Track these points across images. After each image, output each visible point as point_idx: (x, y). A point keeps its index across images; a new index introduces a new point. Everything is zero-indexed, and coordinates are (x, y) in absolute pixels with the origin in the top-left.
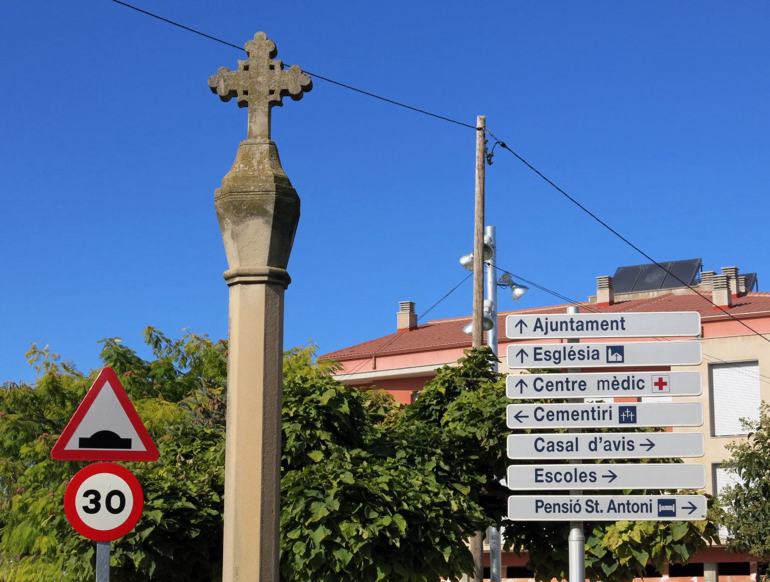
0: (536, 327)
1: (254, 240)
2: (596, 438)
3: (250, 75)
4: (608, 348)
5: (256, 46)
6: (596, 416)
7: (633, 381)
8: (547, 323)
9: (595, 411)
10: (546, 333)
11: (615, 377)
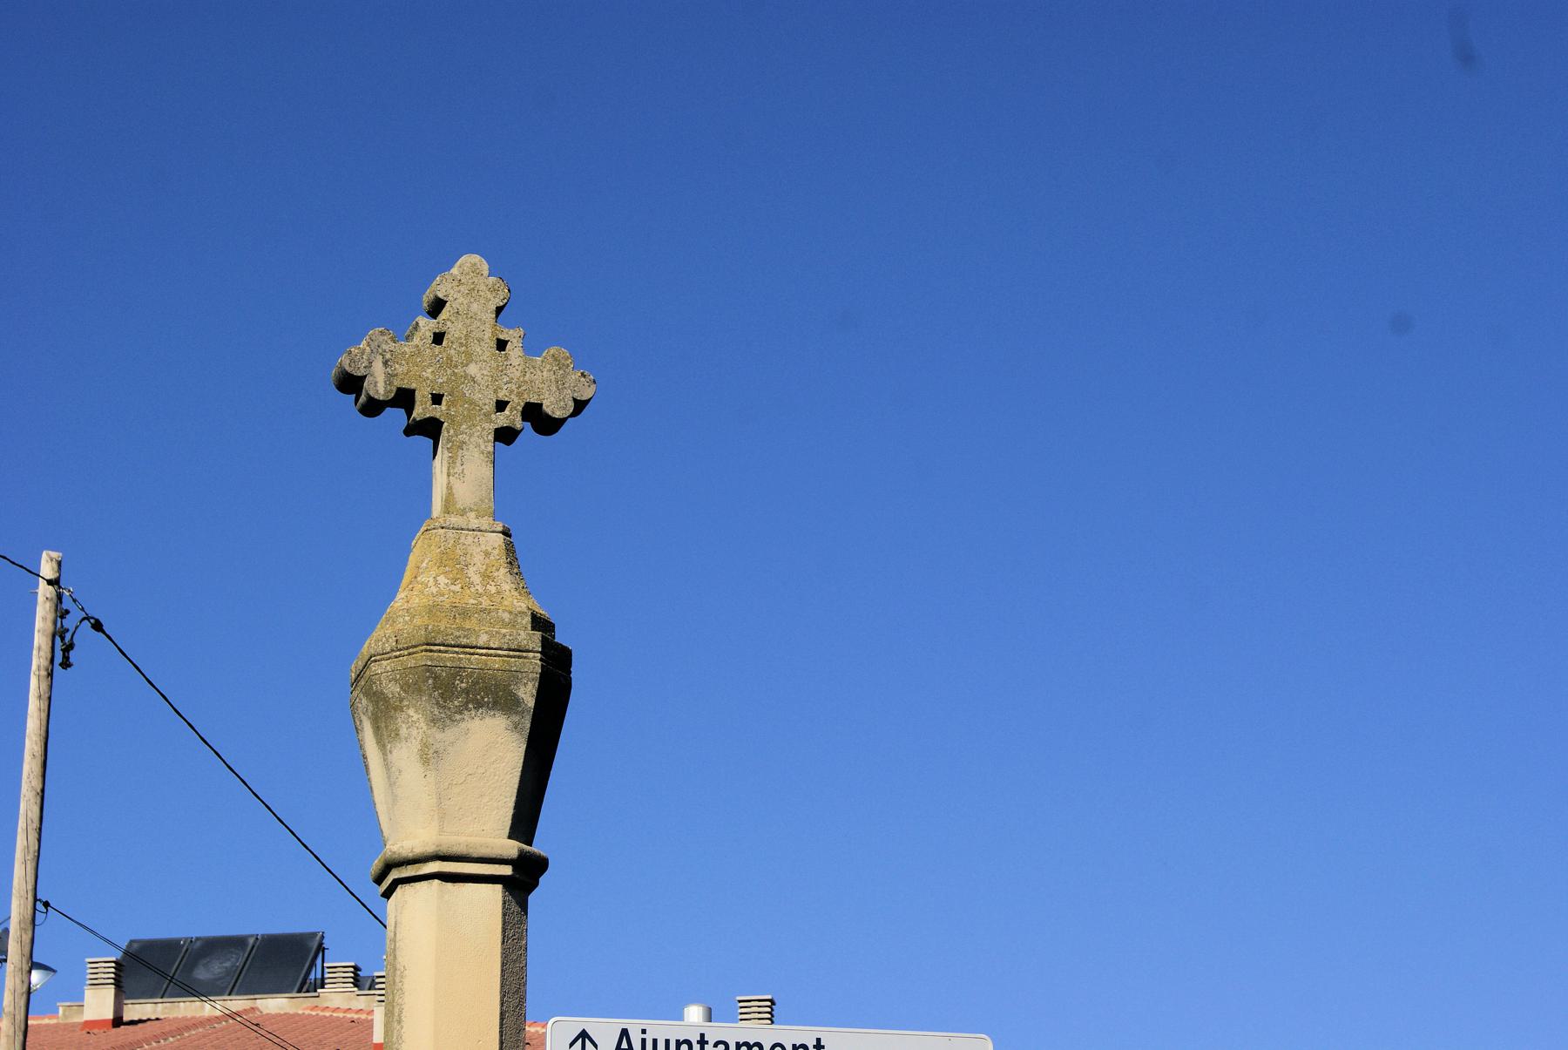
1: (481, 770)
3: (450, 358)
5: (462, 288)
8: (644, 1041)
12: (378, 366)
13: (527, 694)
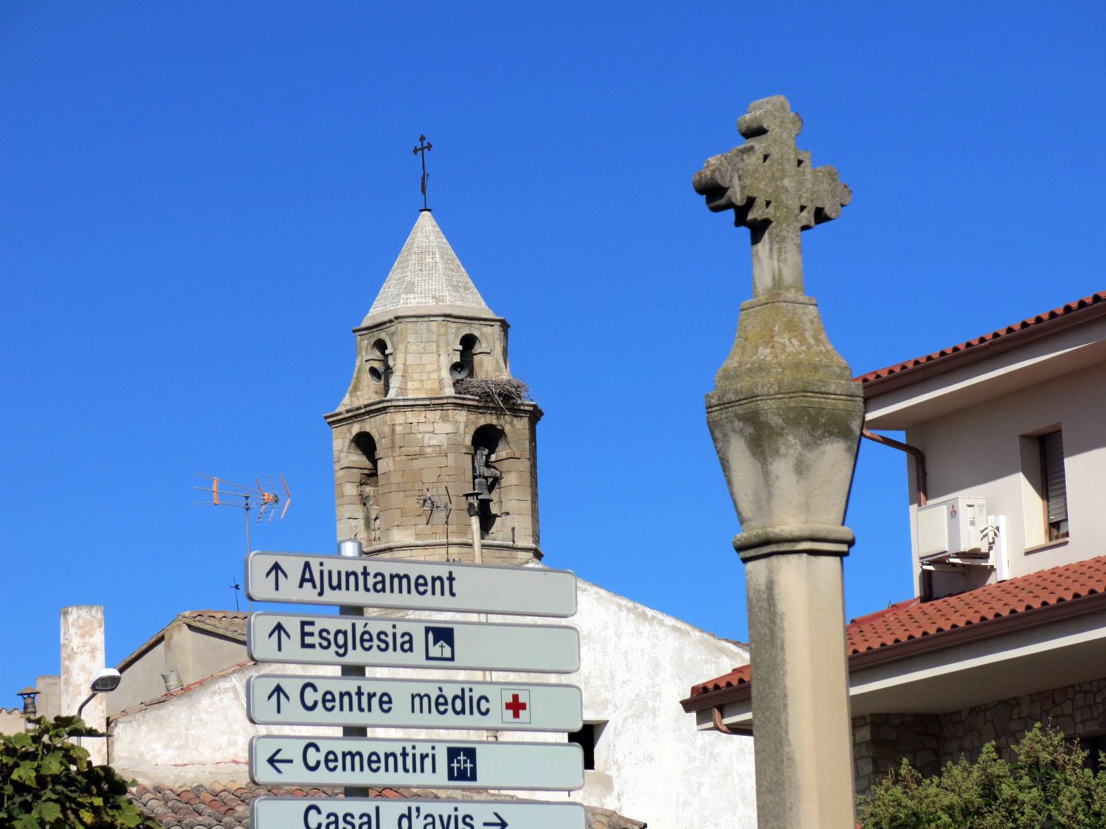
0: (303, 580)
2: (410, 809)
4: (427, 630)
6: (409, 765)
7: (471, 698)
8: (322, 572)
9: (407, 755)
10: (321, 594)
11: (440, 689)
12: (736, 179)
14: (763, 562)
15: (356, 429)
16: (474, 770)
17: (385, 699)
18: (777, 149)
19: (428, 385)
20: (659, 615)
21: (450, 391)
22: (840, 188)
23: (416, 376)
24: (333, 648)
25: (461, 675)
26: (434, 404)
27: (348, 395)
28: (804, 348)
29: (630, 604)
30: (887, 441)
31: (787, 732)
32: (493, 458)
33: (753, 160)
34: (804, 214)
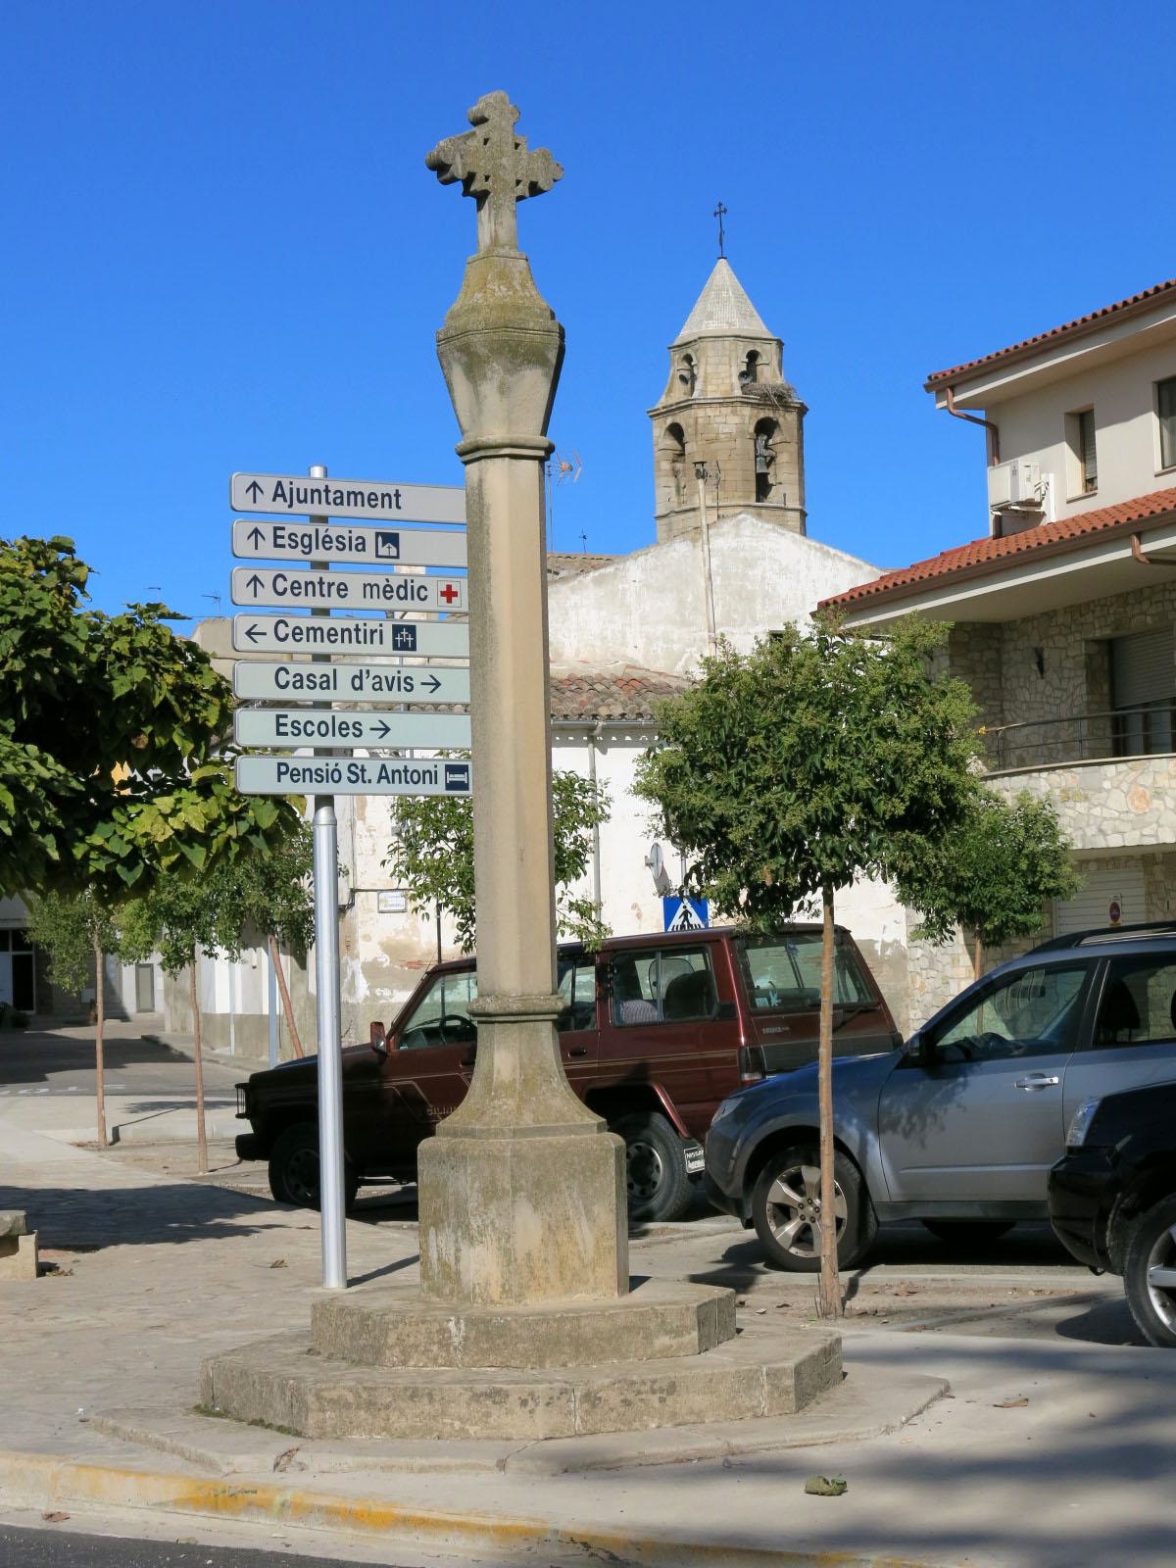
0: (276, 495)
6: (361, 638)
7: (412, 587)
8: (291, 489)
10: (290, 506)
11: (387, 580)
12: (458, 159)
13: (552, 356)
14: (476, 464)
15: (669, 421)
16: (414, 643)
17: (342, 587)
18: (496, 134)
19: (722, 388)
20: (839, 554)
21: (738, 392)
22: (553, 166)
23: (714, 381)
24: (300, 547)
25: (405, 570)
26: (725, 402)
27: (664, 396)
28: (511, 293)
29: (818, 545)
30: (969, 418)
31: (489, 599)
32: (771, 442)
33: (475, 143)
34: (520, 186)
